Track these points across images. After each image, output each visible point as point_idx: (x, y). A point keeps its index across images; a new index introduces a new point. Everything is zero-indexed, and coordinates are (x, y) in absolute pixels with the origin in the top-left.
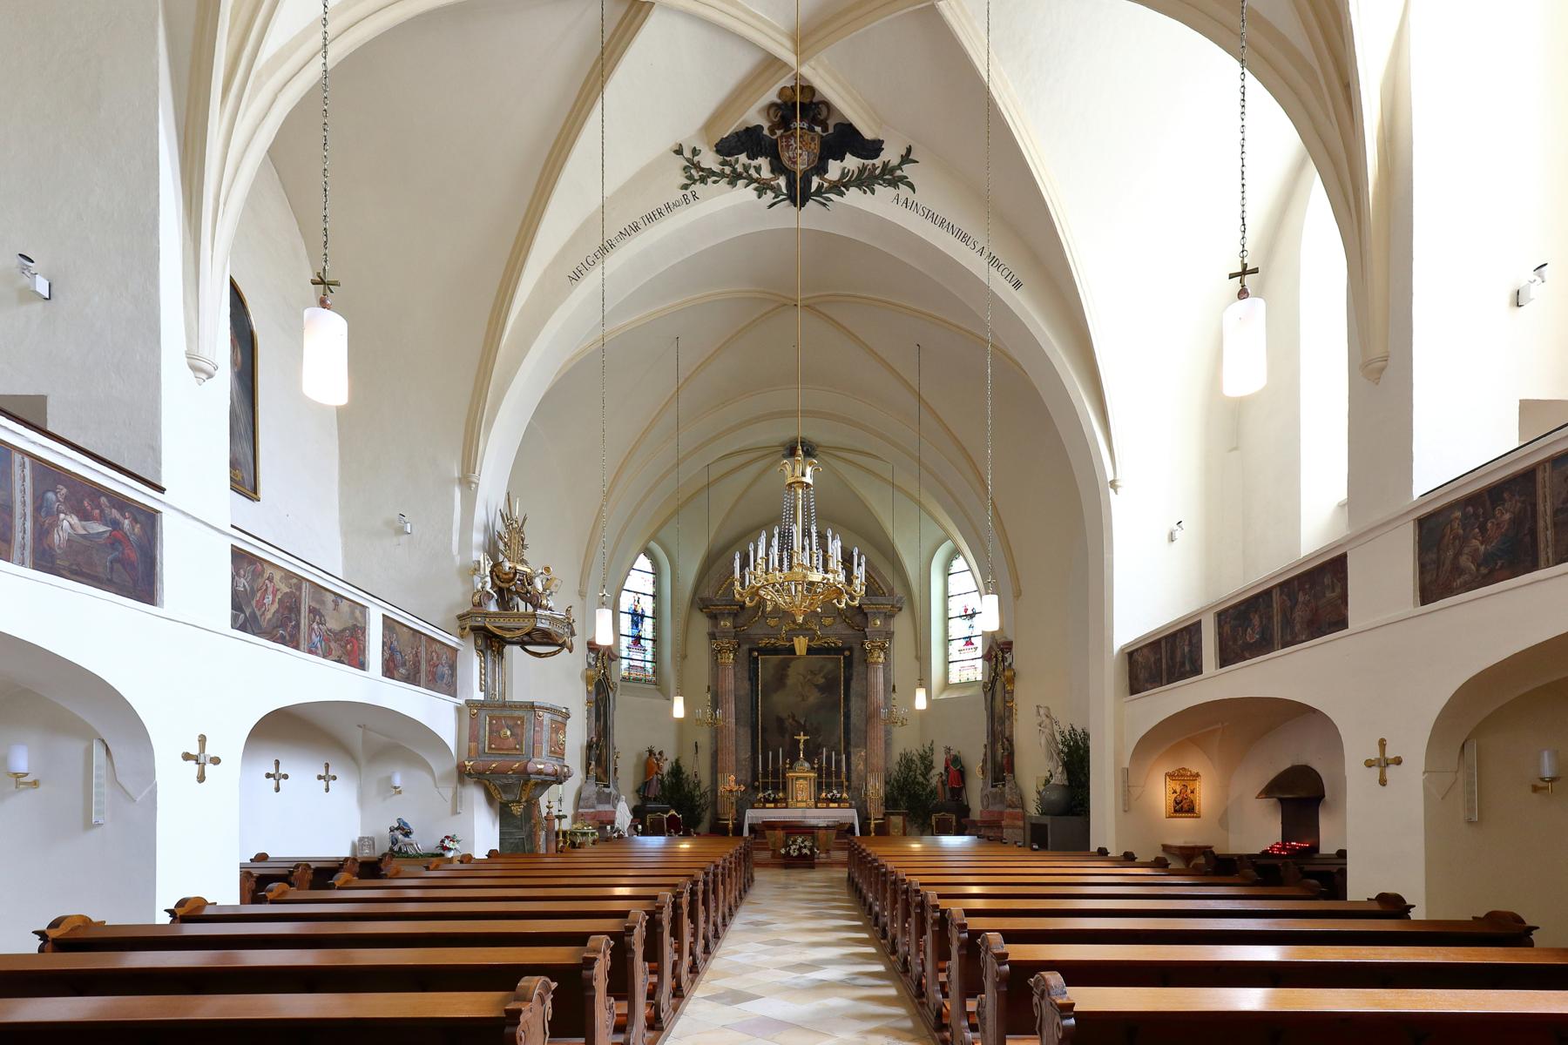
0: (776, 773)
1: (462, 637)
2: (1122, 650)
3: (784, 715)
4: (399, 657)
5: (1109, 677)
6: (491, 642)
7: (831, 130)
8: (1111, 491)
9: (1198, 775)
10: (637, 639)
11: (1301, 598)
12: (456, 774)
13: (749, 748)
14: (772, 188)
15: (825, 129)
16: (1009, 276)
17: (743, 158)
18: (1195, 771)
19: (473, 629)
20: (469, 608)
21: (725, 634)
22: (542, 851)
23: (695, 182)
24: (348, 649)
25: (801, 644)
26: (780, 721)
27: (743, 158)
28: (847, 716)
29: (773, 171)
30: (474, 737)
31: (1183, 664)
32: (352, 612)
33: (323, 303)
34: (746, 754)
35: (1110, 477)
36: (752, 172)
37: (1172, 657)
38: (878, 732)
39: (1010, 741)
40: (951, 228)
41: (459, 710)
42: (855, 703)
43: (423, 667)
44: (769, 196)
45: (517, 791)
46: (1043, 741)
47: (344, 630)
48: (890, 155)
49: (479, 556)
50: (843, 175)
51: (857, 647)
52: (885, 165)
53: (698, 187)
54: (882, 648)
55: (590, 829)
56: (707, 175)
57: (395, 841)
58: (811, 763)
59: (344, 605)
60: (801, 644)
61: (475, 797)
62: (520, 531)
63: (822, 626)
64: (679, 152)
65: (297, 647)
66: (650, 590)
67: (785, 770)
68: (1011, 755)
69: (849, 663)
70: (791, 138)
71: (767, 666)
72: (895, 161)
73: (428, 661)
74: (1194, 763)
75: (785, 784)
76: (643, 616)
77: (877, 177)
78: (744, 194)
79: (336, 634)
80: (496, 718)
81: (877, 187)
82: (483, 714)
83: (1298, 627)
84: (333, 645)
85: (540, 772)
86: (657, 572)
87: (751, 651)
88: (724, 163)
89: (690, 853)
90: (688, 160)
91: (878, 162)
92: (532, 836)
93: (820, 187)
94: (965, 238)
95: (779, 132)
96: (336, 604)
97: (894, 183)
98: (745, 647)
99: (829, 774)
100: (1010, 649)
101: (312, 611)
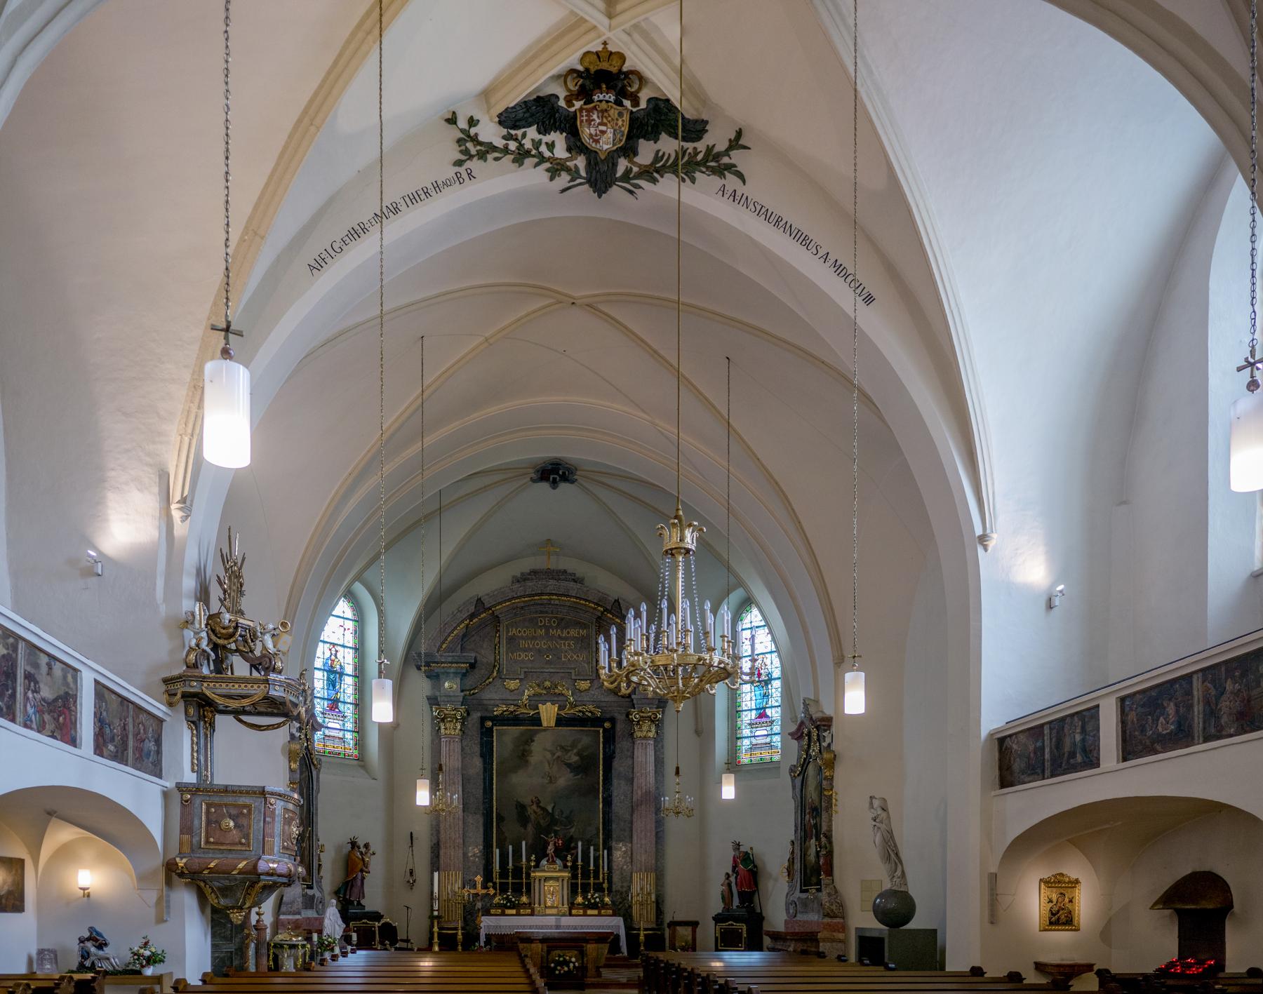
0: (517, 871)
1: (170, 705)
2: (991, 735)
3: (527, 801)
4: (108, 730)
5: (975, 765)
6: (202, 710)
7: (643, 105)
8: (980, 550)
9: (1077, 881)
10: (334, 704)
11: (1229, 686)
12: (162, 876)
13: (480, 840)
14: (568, 170)
15: (636, 102)
16: (858, 287)
17: (532, 132)
18: (1074, 876)
19: (185, 696)
20: (180, 669)
21: (449, 697)
22: (252, 969)
23: (471, 157)
24: (57, 719)
25: (548, 713)
26: (521, 808)
27: (532, 132)
28: (608, 802)
29: (569, 150)
30: (187, 828)
31: (1072, 755)
32: (65, 677)
33: (226, 353)
34: (475, 850)
35: (978, 531)
36: (543, 148)
37: (1059, 745)
38: (643, 824)
39: (829, 837)
40: (788, 229)
41: (166, 795)
42: (619, 788)
43: (131, 743)
44: (564, 179)
45: (240, 895)
46: (878, 839)
47: (55, 700)
48: (717, 138)
49: (189, 605)
50: (657, 158)
51: (620, 718)
52: (709, 150)
53: (474, 164)
54: (653, 721)
55: (298, 940)
56: (486, 150)
57: (85, 955)
58: (564, 860)
59: (57, 668)
60: (548, 713)
61: (186, 900)
62: (239, 577)
63: (576, 691)
64: (452, 120)
65: (13, 720)
66: (350, 640)
67: (529, 868)
68: (830, 854)
69: (610, 738)
70: (601, 120)
71: (504, 739)
72: (721, 146)
73: (136, 734)
74: (1075, 868)
75: (529, 886)
76: (341, 674)
77: (698, 164)
78: (533, 177)
79: (49, 704)
80: (204, 803)
81: (697, 175)
82: (197, 801)
83: (1224, 720)
84: (47, 717)
85: (271, 873)
86: (360, 619)
87: (483, 720)
88: (508, 137)
89: (436, 973)
90: (462, 131)
91: (701, 146)
92: (242, 951)
93: (628, 172)
94: (805, 241)
95: (578, 104)
96: (50, 668)
97: (720, 171)
98: (476, 716)
99: (586, 874)
100: (829, 727)
101: (29, 677)
